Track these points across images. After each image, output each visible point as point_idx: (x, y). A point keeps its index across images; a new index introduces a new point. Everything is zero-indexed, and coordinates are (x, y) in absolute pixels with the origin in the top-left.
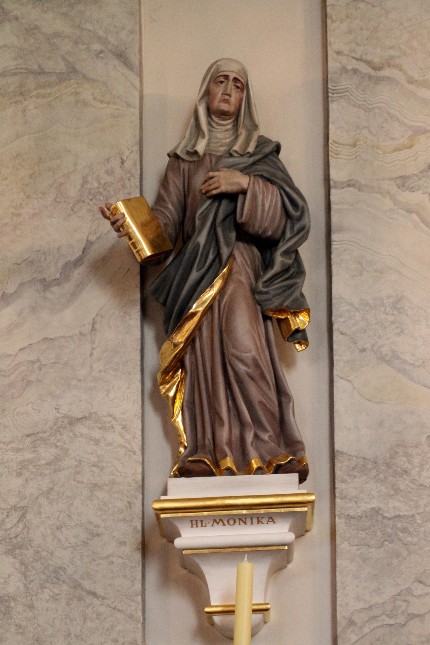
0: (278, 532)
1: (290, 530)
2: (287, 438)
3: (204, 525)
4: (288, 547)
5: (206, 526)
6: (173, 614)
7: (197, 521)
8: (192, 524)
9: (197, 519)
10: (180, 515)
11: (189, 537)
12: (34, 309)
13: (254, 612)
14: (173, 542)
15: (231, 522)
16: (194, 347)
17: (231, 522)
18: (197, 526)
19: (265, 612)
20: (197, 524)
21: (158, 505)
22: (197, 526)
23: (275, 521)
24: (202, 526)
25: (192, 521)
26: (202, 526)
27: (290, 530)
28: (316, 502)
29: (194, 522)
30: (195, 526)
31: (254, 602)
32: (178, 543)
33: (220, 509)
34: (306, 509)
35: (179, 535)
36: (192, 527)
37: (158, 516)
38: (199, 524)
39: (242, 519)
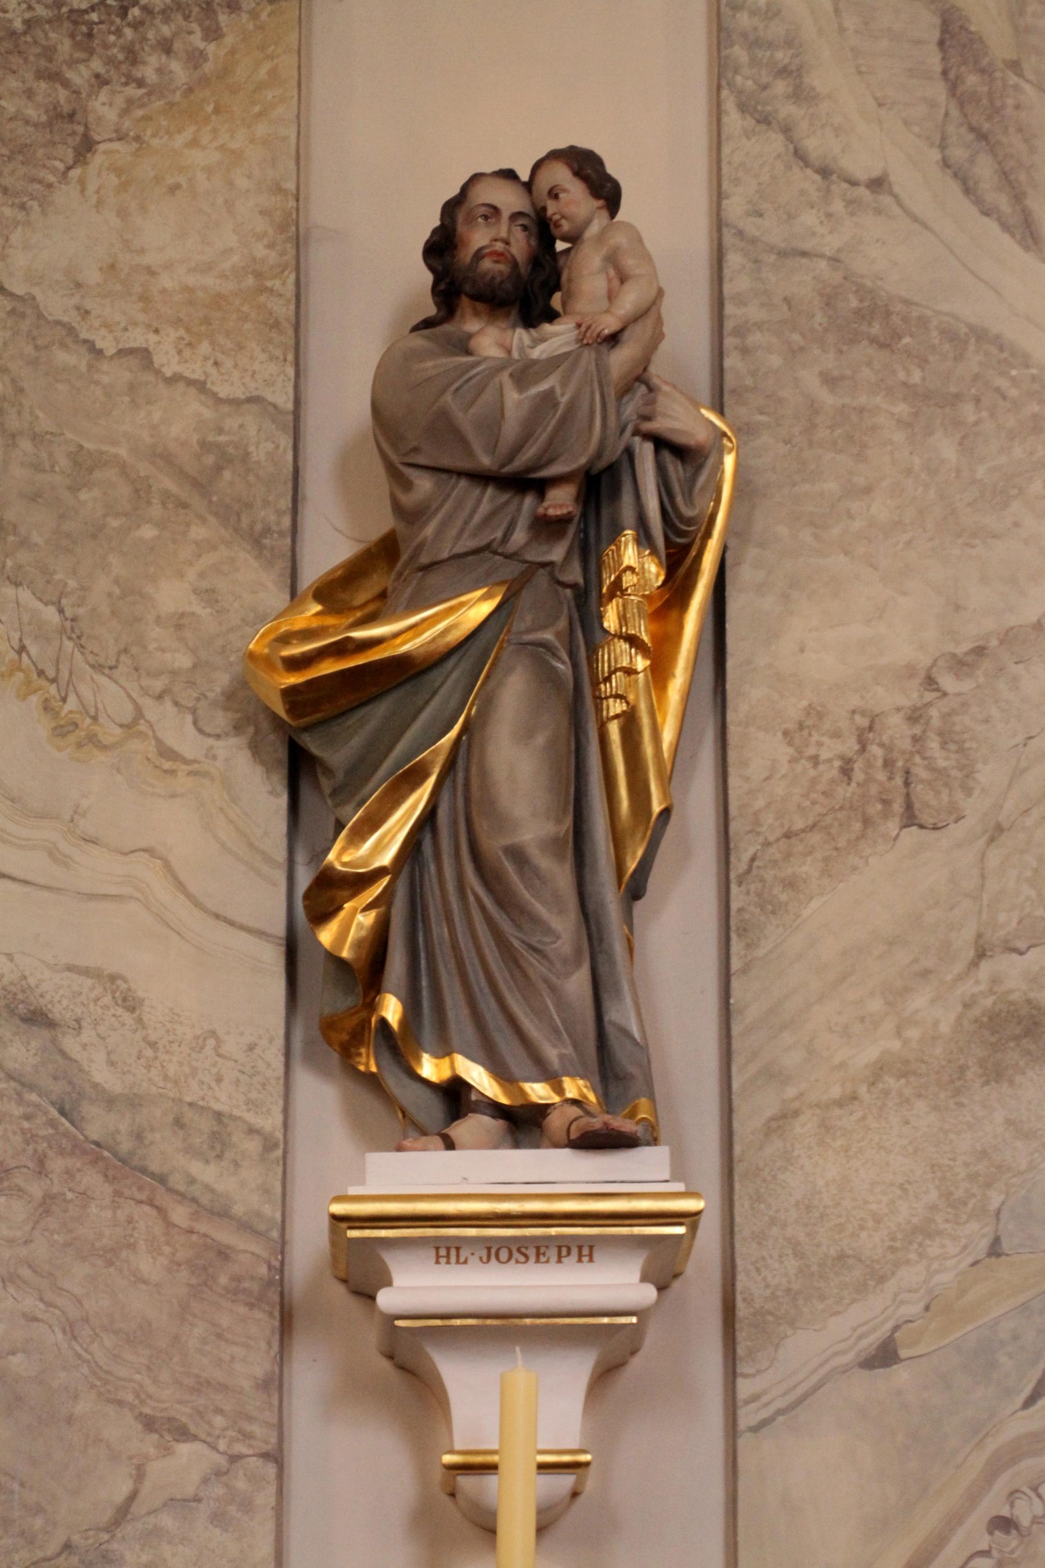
0: (613, 1284)
1: (644, 1279)
2: (612, 1064)
3: (462, 1259)
4: (639, 1320)
5: (465, 1262)
6: (351, 1473)
7: (448, 1249)
8: (438, 1257)
9: (448, 1245)
10: (383, 1233)
11: (415, 1286)
12: (665, 415)
13: (542, 1471)
14: (372, 1298)
15: (504, 1254)
16: (435, 831)
17: (504, 1254)
18: (448, 1262)
19: (579, 1471)
20: (448, 1256)
21: (338, 1209)
22: (448, 1262)
23: (595, 1256)
24: (458, 1262)
25: (437, 1249)
26: (458, 1262)
27: (644, 1279)
28: (704, 1214)
29: (586, 1251)
30: (443, 1260)
31: (541, 1446)
32: (386, 1300)
33: (404, 1224)
34: (680, 1230)
35: (388, 1283)
36: (437, 1262)
37: (336, 1238)
38: (453, 1259)
39: (564, 1249)
